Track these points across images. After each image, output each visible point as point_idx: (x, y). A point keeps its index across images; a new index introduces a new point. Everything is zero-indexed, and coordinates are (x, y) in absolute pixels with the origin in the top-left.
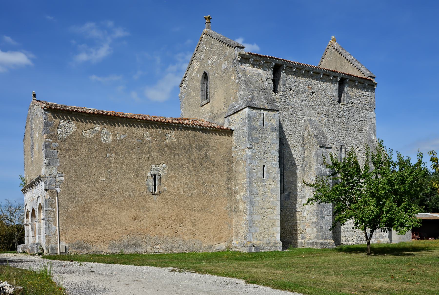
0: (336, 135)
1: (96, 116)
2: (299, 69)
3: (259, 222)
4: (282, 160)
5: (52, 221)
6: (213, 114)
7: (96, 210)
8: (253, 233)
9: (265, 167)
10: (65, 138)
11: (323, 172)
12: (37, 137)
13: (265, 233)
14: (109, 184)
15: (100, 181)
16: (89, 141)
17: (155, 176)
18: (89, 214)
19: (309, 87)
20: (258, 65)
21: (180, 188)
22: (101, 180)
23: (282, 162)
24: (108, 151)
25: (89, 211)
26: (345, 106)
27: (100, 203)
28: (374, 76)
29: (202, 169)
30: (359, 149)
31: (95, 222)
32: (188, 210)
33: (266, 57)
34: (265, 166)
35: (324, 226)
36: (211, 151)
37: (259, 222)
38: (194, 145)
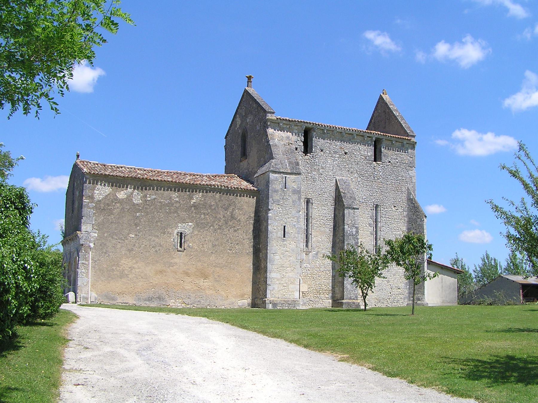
0: (370, 194)
1: (130, 179)
2: (331, 131)
3: (278, 280)
4: (311, 219)
5: (85, 273)
6: (249, 171)
7: (124, 264)
8: (271, 290)
9: (286, 227)
10: (101, 199)
11: (349, 232)
12: (78, 195)
13: (284, 291)
14: (138, 241)
15: (130, 238)
16: (121, 201)
17: (181, 233)
18: (118, 268)
19: (341, 148)
20: (23, 292)
21: (205, 246)
22: (131, 237)
23: (311, 221)
24: (139, 210)
25: (118, 265)
26: (381, 165)
27: (128, 258)
28: (414, 135)
29: (227, 228)
30: (396, 208)
31: (122, 275)
32: (211, 266)
33: (295, 121)
34: (285, 226)
35: (349, 286)
36: (237, 211)
37: (278, 280)
38: (220, 205)
